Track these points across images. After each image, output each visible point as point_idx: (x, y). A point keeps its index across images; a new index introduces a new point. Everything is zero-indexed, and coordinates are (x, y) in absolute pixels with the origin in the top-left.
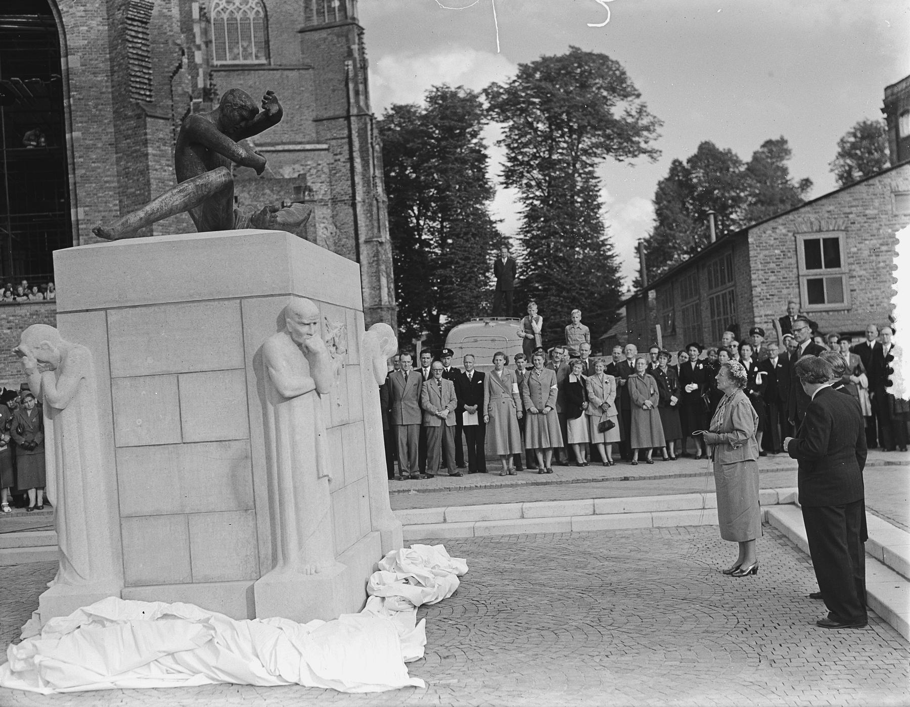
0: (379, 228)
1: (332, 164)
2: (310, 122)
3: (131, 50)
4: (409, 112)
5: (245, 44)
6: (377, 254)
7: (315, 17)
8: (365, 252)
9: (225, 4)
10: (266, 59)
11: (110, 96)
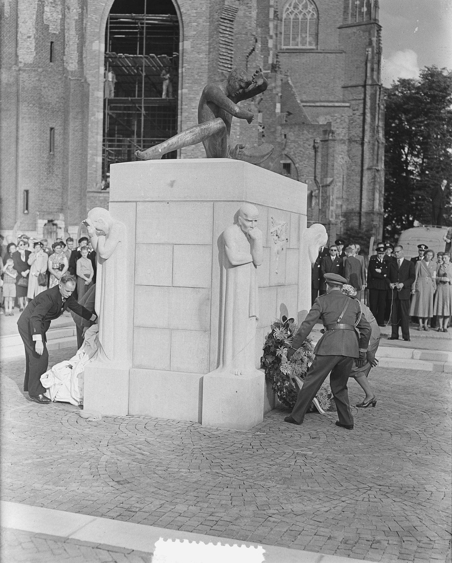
0: (377, 160)
1: (351, 116)
2: (340, 88)
3: (222, 39)
4: (409, 84)
5: (304, 35)
6: (374, 178)
7: (350, 18)
8: (367, 176)
9: (292, 9)
10: (315, 46)
11: (207, 67)
